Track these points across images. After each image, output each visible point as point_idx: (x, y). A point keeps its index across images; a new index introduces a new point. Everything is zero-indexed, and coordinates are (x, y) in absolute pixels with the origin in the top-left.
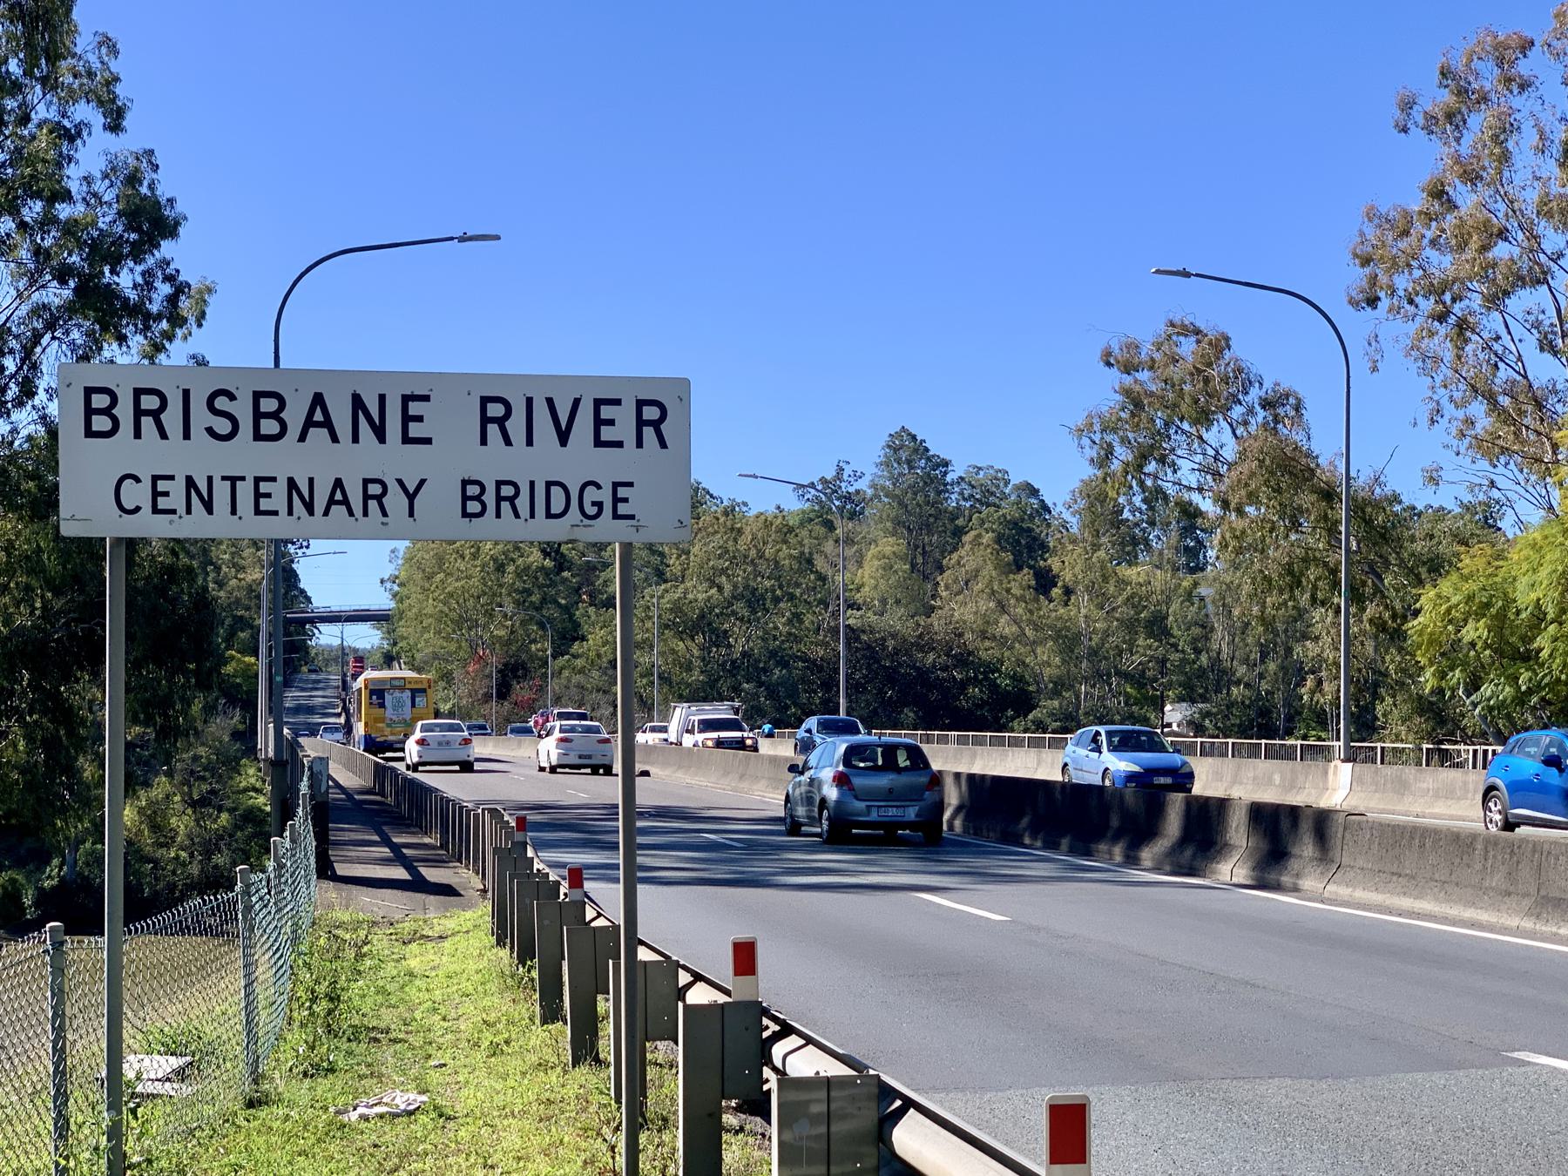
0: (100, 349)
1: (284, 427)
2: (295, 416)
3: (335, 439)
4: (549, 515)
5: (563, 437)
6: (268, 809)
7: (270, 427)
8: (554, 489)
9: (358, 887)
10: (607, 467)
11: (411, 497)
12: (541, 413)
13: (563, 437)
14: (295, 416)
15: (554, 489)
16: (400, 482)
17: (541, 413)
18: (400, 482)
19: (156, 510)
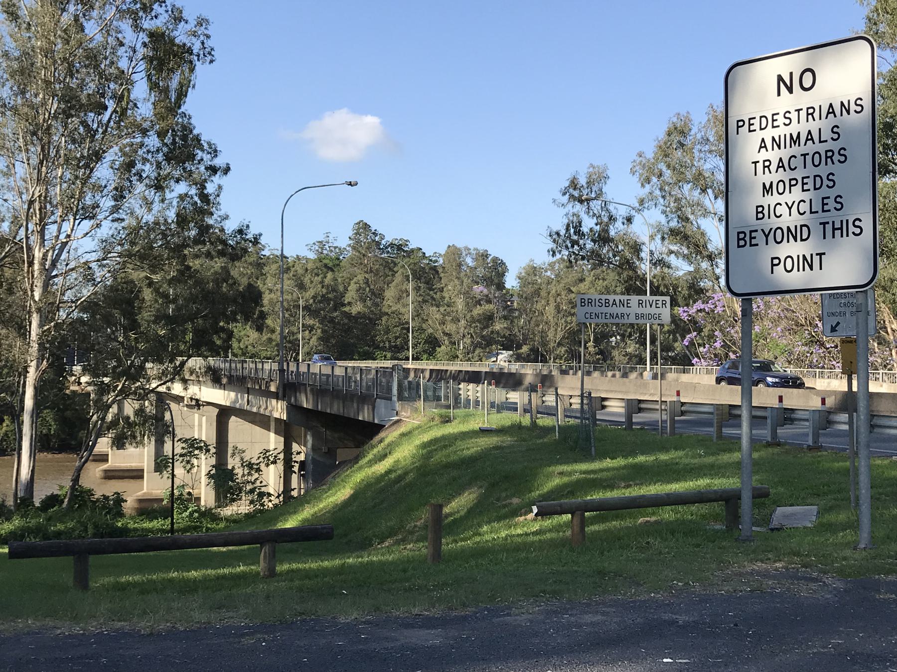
0: (506, 536)
1: (746, 242)
2: (611, 303)
3: (767, 150)
4: (802, 240)
5: (651, 306)
6: (12, 508)
7: (607, 305)
8: (804, 228)
9: (215, 424)
10: (657, 311)
11: (790, 208)
12: (648, 302)
13: (651, 306)
14: (611, 303)
15: (804, 228)
16: (786, 203)
17: (648, 302)
18: (786, 203)
19: (823, 211)
